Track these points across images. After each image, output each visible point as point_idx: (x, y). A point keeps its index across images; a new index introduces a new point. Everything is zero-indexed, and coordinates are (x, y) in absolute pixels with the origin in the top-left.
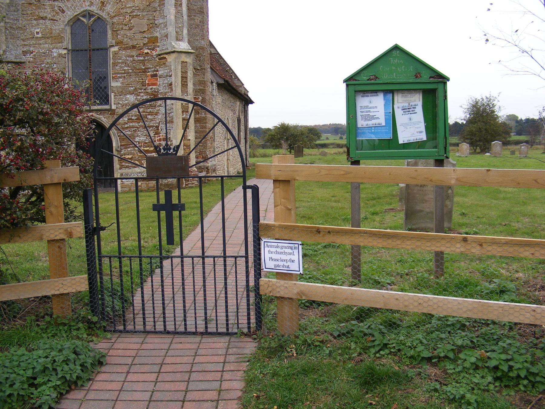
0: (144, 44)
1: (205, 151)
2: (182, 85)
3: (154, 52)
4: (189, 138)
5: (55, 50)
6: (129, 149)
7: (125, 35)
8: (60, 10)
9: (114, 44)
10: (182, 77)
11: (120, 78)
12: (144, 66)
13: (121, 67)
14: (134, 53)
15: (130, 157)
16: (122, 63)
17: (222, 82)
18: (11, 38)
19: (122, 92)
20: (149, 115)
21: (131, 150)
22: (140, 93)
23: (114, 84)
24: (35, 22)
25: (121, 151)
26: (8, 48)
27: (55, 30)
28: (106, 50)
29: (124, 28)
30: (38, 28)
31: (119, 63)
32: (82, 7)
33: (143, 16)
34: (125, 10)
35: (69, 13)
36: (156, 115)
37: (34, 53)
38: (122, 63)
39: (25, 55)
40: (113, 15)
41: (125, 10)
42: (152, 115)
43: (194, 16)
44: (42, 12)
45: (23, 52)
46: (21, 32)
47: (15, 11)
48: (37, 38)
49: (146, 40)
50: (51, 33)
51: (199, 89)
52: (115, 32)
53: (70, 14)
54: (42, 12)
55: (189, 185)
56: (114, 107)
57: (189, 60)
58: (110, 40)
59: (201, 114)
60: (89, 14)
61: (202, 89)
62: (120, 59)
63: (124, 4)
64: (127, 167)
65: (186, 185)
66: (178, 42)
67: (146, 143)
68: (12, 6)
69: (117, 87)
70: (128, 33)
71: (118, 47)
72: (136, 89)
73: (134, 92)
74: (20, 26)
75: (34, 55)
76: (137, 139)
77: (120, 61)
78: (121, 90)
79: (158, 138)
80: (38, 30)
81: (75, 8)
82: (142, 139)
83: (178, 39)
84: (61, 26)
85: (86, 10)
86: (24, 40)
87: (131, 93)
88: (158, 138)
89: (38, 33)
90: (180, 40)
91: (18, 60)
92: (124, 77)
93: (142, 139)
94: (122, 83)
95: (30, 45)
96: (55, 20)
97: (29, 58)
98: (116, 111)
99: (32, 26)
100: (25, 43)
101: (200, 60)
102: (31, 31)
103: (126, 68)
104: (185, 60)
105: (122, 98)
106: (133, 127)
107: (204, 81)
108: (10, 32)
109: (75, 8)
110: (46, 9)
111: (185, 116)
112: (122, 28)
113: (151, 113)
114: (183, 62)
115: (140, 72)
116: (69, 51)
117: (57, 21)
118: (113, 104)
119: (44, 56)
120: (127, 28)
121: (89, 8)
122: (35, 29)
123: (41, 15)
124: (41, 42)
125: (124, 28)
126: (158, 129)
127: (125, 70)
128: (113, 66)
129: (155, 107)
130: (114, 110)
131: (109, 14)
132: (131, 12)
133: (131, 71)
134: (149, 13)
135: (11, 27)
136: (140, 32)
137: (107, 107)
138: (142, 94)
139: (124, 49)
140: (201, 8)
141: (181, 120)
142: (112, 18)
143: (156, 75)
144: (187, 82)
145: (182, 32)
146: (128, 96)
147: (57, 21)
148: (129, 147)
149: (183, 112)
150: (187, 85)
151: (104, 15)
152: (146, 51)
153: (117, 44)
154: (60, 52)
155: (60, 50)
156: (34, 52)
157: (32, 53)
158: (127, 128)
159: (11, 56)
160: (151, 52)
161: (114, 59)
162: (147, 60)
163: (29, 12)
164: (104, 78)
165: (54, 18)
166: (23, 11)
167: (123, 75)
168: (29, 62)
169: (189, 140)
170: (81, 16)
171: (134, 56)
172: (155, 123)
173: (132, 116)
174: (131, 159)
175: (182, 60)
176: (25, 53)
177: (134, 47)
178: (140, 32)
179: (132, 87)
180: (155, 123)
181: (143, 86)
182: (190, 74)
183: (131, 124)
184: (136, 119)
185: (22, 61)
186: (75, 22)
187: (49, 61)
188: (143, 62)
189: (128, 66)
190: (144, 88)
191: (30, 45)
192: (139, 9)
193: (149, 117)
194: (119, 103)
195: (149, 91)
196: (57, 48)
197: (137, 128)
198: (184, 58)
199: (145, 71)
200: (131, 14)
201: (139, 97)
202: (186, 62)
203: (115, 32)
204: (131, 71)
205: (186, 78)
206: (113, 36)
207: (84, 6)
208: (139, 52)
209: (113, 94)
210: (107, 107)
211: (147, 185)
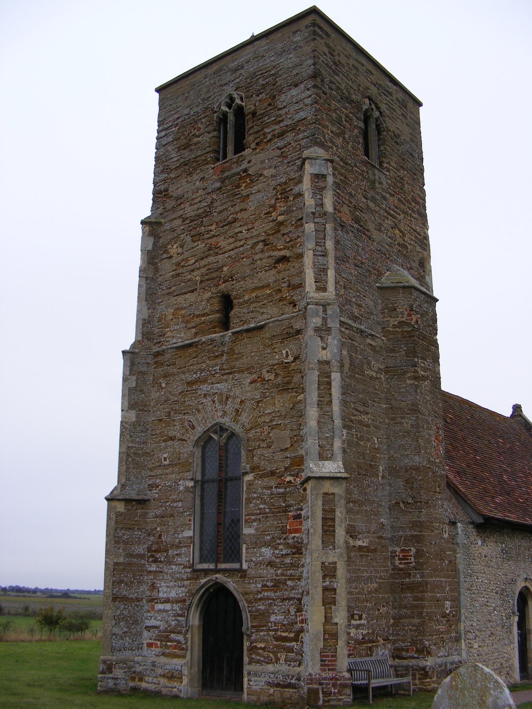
0: (286, 468)
1: (421, 640)
2: (324, 531)
3: (298, 479)
4: (336, 620)
5: (181, 482)
6: (262, 634)
7: (262, 455)
8: (189, 425)
9: (248, 469)
10: (324, 519)
11: (255, 521)
12: (284, 502)
13: (256, 505)
14: (273, 482)
15: (263, 645)
16: (257, 498)
17: (480, 520)
18: (134, 468)
19: (257, 543)
20: (289, 579)
21: (264, 635)
22: (278, 544)
23: (247, 531)
24: (163, 444)
25: (251, 636)
26: (129, 480)
27: (183, 453)
28: (238, 479)
29: (262, 446)
30: (166, 452)
31: (254, 498)
32: (213, 418)
33: (285, 425)
34: (262, 419)
35: (199, 429)
36: (299, 579)
37: (160, 487)
38: (257, 498)
39: (150, 490)
40: (248, 427)
41: (262, 419)
42: (293, 580)
43: (401, 418)
44: (171, 430)
45: (149, 485)
46: (149, 459)
47: (142, 432)
48: (164, 466)
49: (288, 461)
50: (179, 459)
51: (411, 536)
52: (250, 452)
53: (200, 430)
54: (171, 430)
55: (332, 703)
56: (245, 566)
57: (338, 490)
58: (245, 465)
59: (415, 577)
60: (221, 429)
61: (417, 535)
62: (255, 493)
63: (262, 409)
64: (258, 662)
65: (324, 701)
66: (320, 463)
67: (284, 625)
68: (140, 425)
69: (250, 534)
70: (267, 453)
71: (252, 474)
72: (273, 538)
73: (272, 544)
74: (148, 451)
75: (160, 490)
76: (273, 618)
77: (255, 495)
78: (255, 540)
79: (301, 618)
80: (166, 455)
81: (206, 421)
82: (278, 618)
83: (322, 457)
84: (188, 449)
85: (217, 424)
86: (151, 470)
87: (267, 545)
88: (301, 618)
89: (165, 459)
90: (327, 459)
91: (140, 498)
92: (260, 520)
93: (278, 618)
94: (256, 529)
95: (156, 476)
96: (184, 440)
97: (154, 494)
98: (248, 573)
99: (160, 450)
100: (152, 474)
101: (412, 488)
102: (159, 457)
103: (262, 506)
104: (331, 491)
105: (256, 553)
106: (268, 598)
107: (420, 522)
108: (133, 460)
109: (206, 421)
110: (175, 425)
111: (328, 583)
112: (259, 447)
113: (292, 578)
114: (326, 494)
115: (279, 512)
116: (196, 482)
117: (186, 441)
118: (244, 561)
119: (170, 491)
120: (265, 446)
121: (221, 420)
122: (163, 453)
123: (171, 434)
124: (167, 471)
125: (262, 446)
126: (300, 604)
127: (260, 509)
128: (247, 503)
129: (298, 567)
130: (245, 571)
131: (244, 426)
132: (271, 421)
133: (267, 510)
134: (293, 420)
135: (135, 453)
136: (282, 450)
137: (236, 566)
138: (281, 547)
139: (261, 477)
140: (413, 405)
141: (320, 590)
142: (248, 431)
143: (299, 516)
144: (334, 526)
145: (332, 445)
146: (263, 550)
147: (186, 441)
148: (262, 631)
149: (324, 577)
150: (334, 531)
151: (237, 429)
152: (288, 479)
153: (253, 469)
154: (187, 485)
155: (187, 482)
156: (160, 485)
157: (158, 487)
158: (261, 599)
159: (131, 492)
160: (295, 480)
161: (248, 493)
162: (290, 491)
163: (158, 432)
164: (236, 523)
165: (183, 438)
166: (152, 430)
167: (258, 517)
168: (154, 499)
169: (336, 624)
170: (213, 432)
171: (272, 487)
172: (297, 594)
173: (267, 581)
174: (263, 649)
175: (326, 490)
176: (151, 487)
177: (273, 473)
178: (282, 450)
179: (269, 535)
180: (297, 594)
181: (283, 533)
182: (339, 514)
183: (266, 594)
184: (272, 586)
185: (146, 498)
186: (205, 441)
187: (175, 497)
188: (283, 496)
189: (265, 503)
190: (284, 536)
191: (156, 476)
192: (281, 415)
193: (289, 583)
194: (252, 561)
195: (290, 541)
196: (184, 479)
197: (273, 599)
198: (327, 487)
199: (286, 510)
200: (270, 424)
201: (277, 552)
202: (333, 494)
203: (250, 452)
204: (267, 510)
205: (333, 520)
206: (247, 458)
207: (216, 417)
208: (279, 480)
209: (244, 546)
210: (236, 566)
211: (282, 693)
